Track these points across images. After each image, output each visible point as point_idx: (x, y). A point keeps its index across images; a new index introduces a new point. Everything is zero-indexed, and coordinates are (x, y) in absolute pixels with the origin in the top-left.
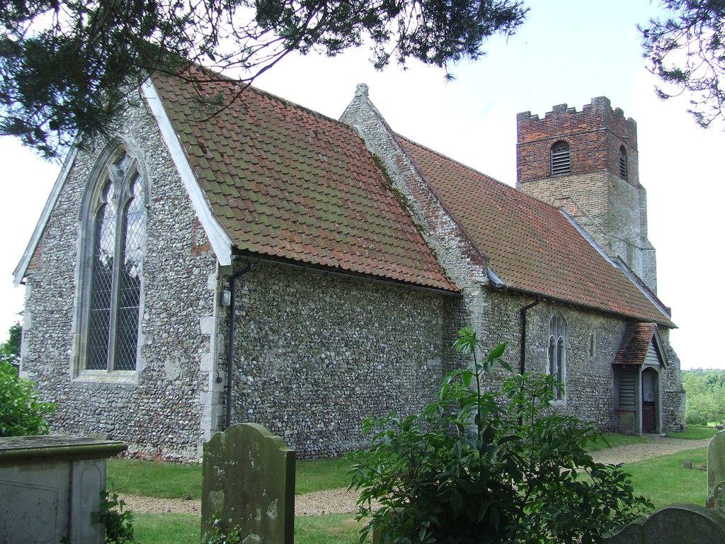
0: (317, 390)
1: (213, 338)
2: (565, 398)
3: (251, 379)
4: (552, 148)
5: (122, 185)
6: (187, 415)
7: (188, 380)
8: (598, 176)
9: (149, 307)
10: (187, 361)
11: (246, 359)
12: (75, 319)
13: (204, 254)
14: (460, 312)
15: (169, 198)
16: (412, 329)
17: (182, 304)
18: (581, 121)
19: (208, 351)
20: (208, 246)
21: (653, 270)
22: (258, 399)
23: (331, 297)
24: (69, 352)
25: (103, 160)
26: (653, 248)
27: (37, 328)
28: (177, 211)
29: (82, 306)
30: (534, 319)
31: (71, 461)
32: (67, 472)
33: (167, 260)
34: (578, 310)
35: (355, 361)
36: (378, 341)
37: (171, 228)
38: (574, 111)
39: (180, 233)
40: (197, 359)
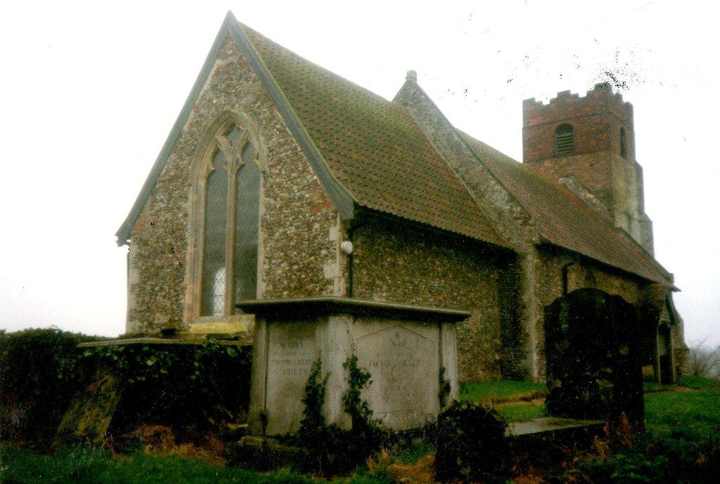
33: (286, 217)
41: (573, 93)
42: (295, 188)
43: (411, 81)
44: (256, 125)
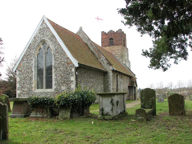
1: (74, 81)
4: (109, 39)
8: (120, 46)
13: (70, 64)
18: (116, 34)
19: (73, 84)
20: (72, 63)
21: (130, 66)
24: (32, 86)
25: (39, 44)
28: (62, 55)
31: (124, 94)
32: (123, 97)
37: (61, 59)
38: (114, 32)
41: (136, 77)
42: (63, 59)
43: (81, 29)
44: (51, 42)
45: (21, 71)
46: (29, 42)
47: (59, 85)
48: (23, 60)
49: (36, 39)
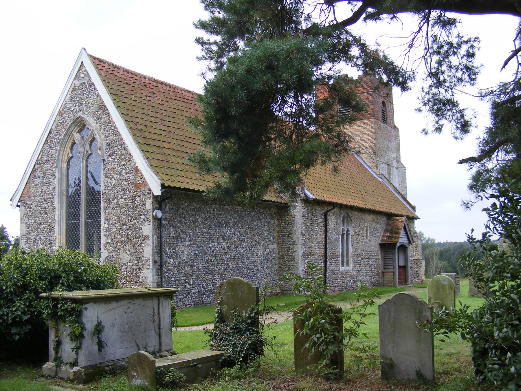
0: (208, 266)
1: (151, 238)
2: (351, 265)
3: (172, 260)
5: (84, 145)
6: (136, 282)
7: (136, 262)
8: (368, 121)
9: (108, 220)
10: (135, 251)
11: (169, 249)
12: (56, 227)
13: (142, 188)
14: (288, 216)
15: (117, 154)
16: (260, 227)
17: (130, 218)
19: (148, 245)
20: (145, 184)
21: (405, 181)
22: (176, 272)
23: (214, 210)
25: (71, 130)
26: (404, 167)
27: (30, 234)
28: (123, 163)
29: (61, 220)
30: (332, 219)
33: (118, 192)
34: (358, 211)
35: (228, 247)
36: (241, 235)
37: (120, 173)
39: (126, 176)
40: (141, 250)
42: (124, 171)
45: (29, 206)
46: (48, 124)
47: (115, 247)
48: (35, 177)
49: (64, 116)
